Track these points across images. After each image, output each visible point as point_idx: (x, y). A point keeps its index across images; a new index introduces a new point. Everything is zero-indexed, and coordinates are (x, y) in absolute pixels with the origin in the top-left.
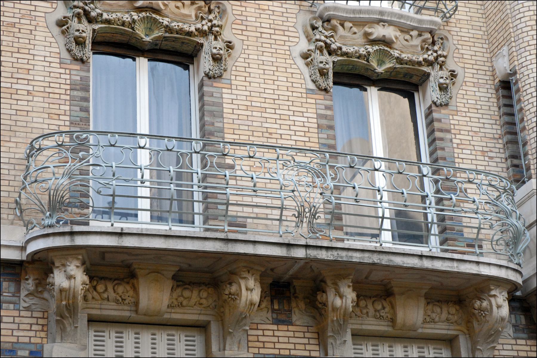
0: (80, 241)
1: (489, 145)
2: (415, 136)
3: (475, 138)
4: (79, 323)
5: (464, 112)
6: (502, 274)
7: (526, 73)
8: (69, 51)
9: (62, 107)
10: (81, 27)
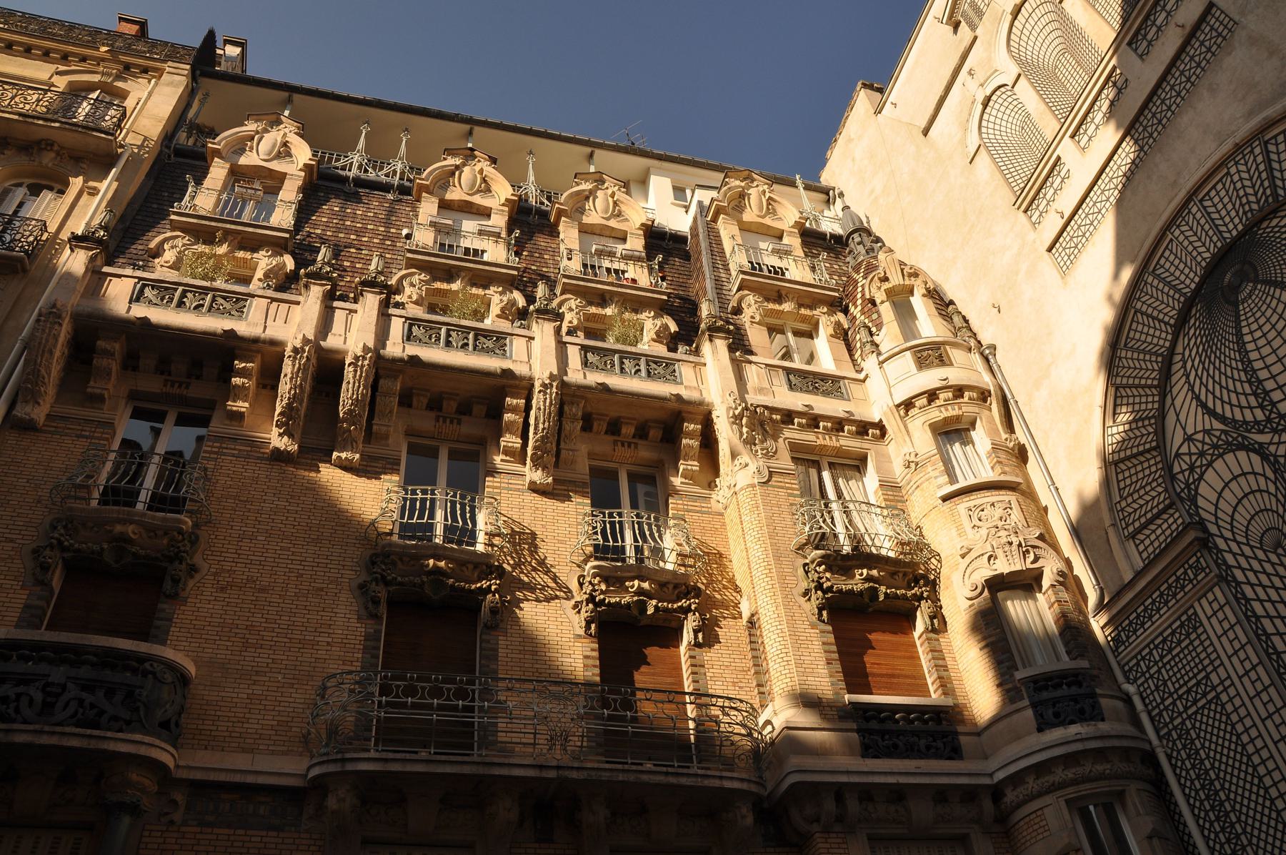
0: (350, 767)
6: (745, 786)
8: (366, 608)
9: (356, 655)
10: (378, 588)
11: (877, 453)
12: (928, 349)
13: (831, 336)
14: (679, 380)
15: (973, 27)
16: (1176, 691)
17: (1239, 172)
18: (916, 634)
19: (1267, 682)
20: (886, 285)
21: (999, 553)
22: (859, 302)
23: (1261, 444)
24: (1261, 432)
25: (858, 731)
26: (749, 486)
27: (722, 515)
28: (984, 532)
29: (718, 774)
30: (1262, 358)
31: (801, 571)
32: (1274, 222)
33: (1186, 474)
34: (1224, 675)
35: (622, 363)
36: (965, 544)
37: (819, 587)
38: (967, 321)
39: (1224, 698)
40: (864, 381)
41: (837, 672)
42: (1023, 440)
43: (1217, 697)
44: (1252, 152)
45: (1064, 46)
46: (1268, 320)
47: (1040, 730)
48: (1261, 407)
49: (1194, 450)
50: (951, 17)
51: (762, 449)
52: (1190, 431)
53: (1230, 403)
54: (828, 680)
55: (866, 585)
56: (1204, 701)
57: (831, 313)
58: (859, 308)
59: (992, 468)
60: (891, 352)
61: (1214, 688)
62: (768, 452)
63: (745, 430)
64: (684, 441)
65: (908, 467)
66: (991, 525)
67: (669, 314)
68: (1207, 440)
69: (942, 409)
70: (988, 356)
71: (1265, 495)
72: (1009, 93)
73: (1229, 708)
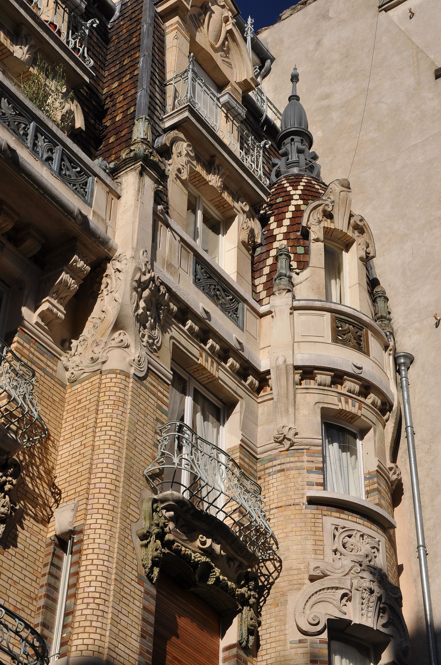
1: (23, 602)
2: (403, 489)
3: (12, 589)
4: (150, 557)
5: (11, 554)
7: (92, 536)
11: (247, 406)
12: (350, 323)
13: (243, 243)
14: (88, 198)
18: (224, 643)
20: (327, 223)
21: (356, 596)
22: (286, 222)
26: (122, 372)
27: (64, 386)
31: (147, 506)
35: (36, 137)
36: (323, 566)
37: (161, 536)
40: (261, 316)
41: (148, 652)
51: (150, 337)
54: (136, 657)
55: (204, 559)
57: (250, 215)
58: (284, 229)
60: (310, 304)
62: (153, 344)
63: (142, 304)
64: (64, 276)
65: (281, 442)
66: (355, 559)
67: (80, 101)
69: (343, 399)
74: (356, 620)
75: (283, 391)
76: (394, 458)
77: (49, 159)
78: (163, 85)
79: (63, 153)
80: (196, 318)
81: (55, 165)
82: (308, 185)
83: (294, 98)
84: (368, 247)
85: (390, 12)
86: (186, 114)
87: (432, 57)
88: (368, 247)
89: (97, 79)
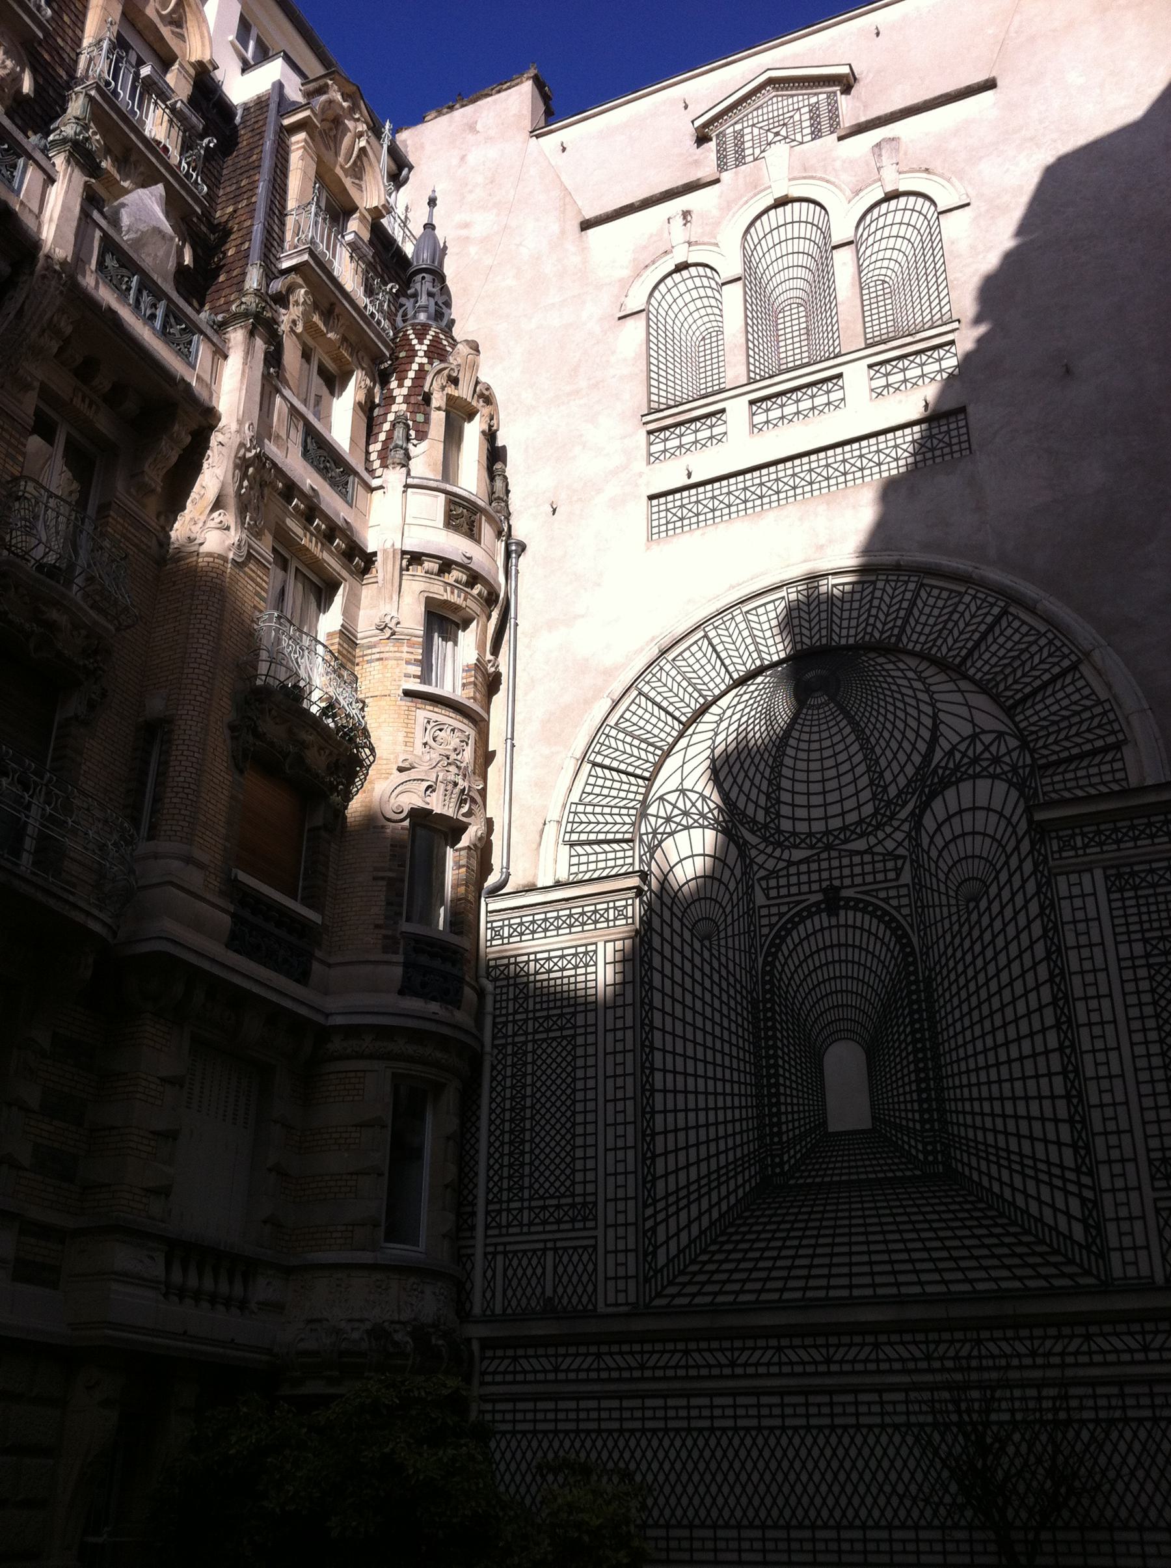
11: (351, 589)
12: (464, 507)
13: (359, 404)
15: (722, 166)
16: (535, 1011)
17: (884, 590)
19: (629, 1046)
20: (451, 390)
21: (441, 788)
22: (408, 383)
23: (746, 842)
24: (753, 832)
25: (233, 916)
28: (435, 756)
29: (86, 907)
30: (794, 769)
32: (881, 660)
33: (660, 821)
34: (591, 1021)
38: (508, 492)
39: (580, 1040)
40: (372, 490)
42: (503, 669)
43: (574, 1036)
44: (906, 582)
45: (805, 296)
46: (820, 740)
47: (401, 992)
48: (767, 811)
49: (680, 804)
50: (706, 125)
52: (687, 785)
53: (740, 788)
56: (558, 1034)
58: (405, 391)
59: (464, 685)
60: (425, 483)
61: (575, 1027)
68: (699, 804)
70: (514, 550)
71: (723, 888)
72: (713, 285)
73: (580, 1052)
74: (438, 809)
75: (389, 576)
76: (496, 650)
77: (153, 317)
78: (283, 215)
79: (168, 309)
80: (303, 495)
81: (158, 324)
82: (436, 341)
83: (429, 226)
84: (492, 419)
85: (541, 139)
86: (306, 257)
87: (580, 203)
88: (492, 419)
89: (211, 197)
